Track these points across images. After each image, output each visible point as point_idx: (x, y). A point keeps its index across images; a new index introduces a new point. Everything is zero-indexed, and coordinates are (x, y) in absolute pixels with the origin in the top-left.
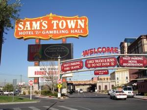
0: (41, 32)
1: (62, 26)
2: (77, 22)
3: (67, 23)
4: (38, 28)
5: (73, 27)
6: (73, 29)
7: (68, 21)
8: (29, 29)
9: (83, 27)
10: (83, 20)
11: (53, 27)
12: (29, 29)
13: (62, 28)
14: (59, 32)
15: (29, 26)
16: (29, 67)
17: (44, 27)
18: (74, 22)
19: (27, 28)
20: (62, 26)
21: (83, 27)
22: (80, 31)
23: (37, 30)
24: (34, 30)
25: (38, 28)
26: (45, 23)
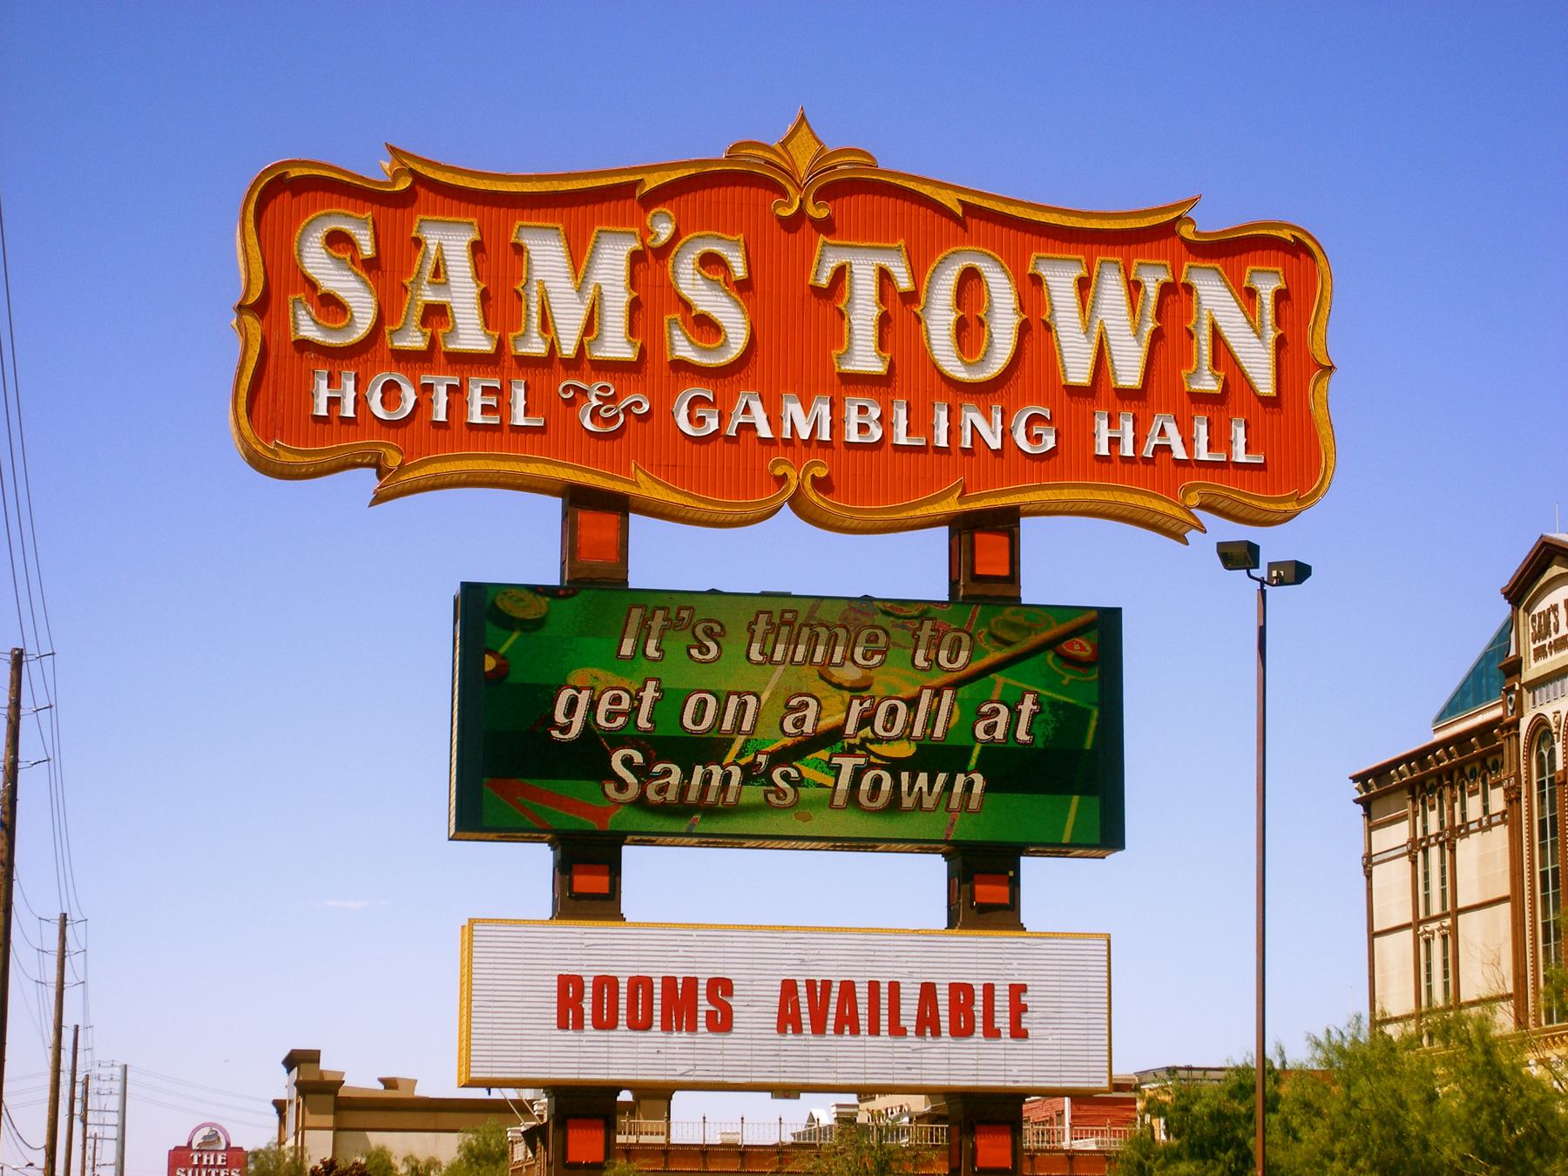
0: (661, 414)
1: (969, 332)
2: (1176, 294)
3: (1031, 290)
4: (616, 345)
5: (1129, 371)
6: (1125, 395)
7: (1061, 281)
8: (471, 336)
9: (1265, 384)
10: (1266, 288)
11: (836, 329)
12: (471, 336)
13: (955, 368)
14: (920, 422)
15: (463, 295)
16: (1022, 858)
17: (706, 327)
18: (1134, 287)
19: (436, 314)
20: (969, 332)
21: (1265, 384)
22: (1219, 440)
23: (579, 363)
24: (550, 362)
25: (616, 345)
26: (710, 262)
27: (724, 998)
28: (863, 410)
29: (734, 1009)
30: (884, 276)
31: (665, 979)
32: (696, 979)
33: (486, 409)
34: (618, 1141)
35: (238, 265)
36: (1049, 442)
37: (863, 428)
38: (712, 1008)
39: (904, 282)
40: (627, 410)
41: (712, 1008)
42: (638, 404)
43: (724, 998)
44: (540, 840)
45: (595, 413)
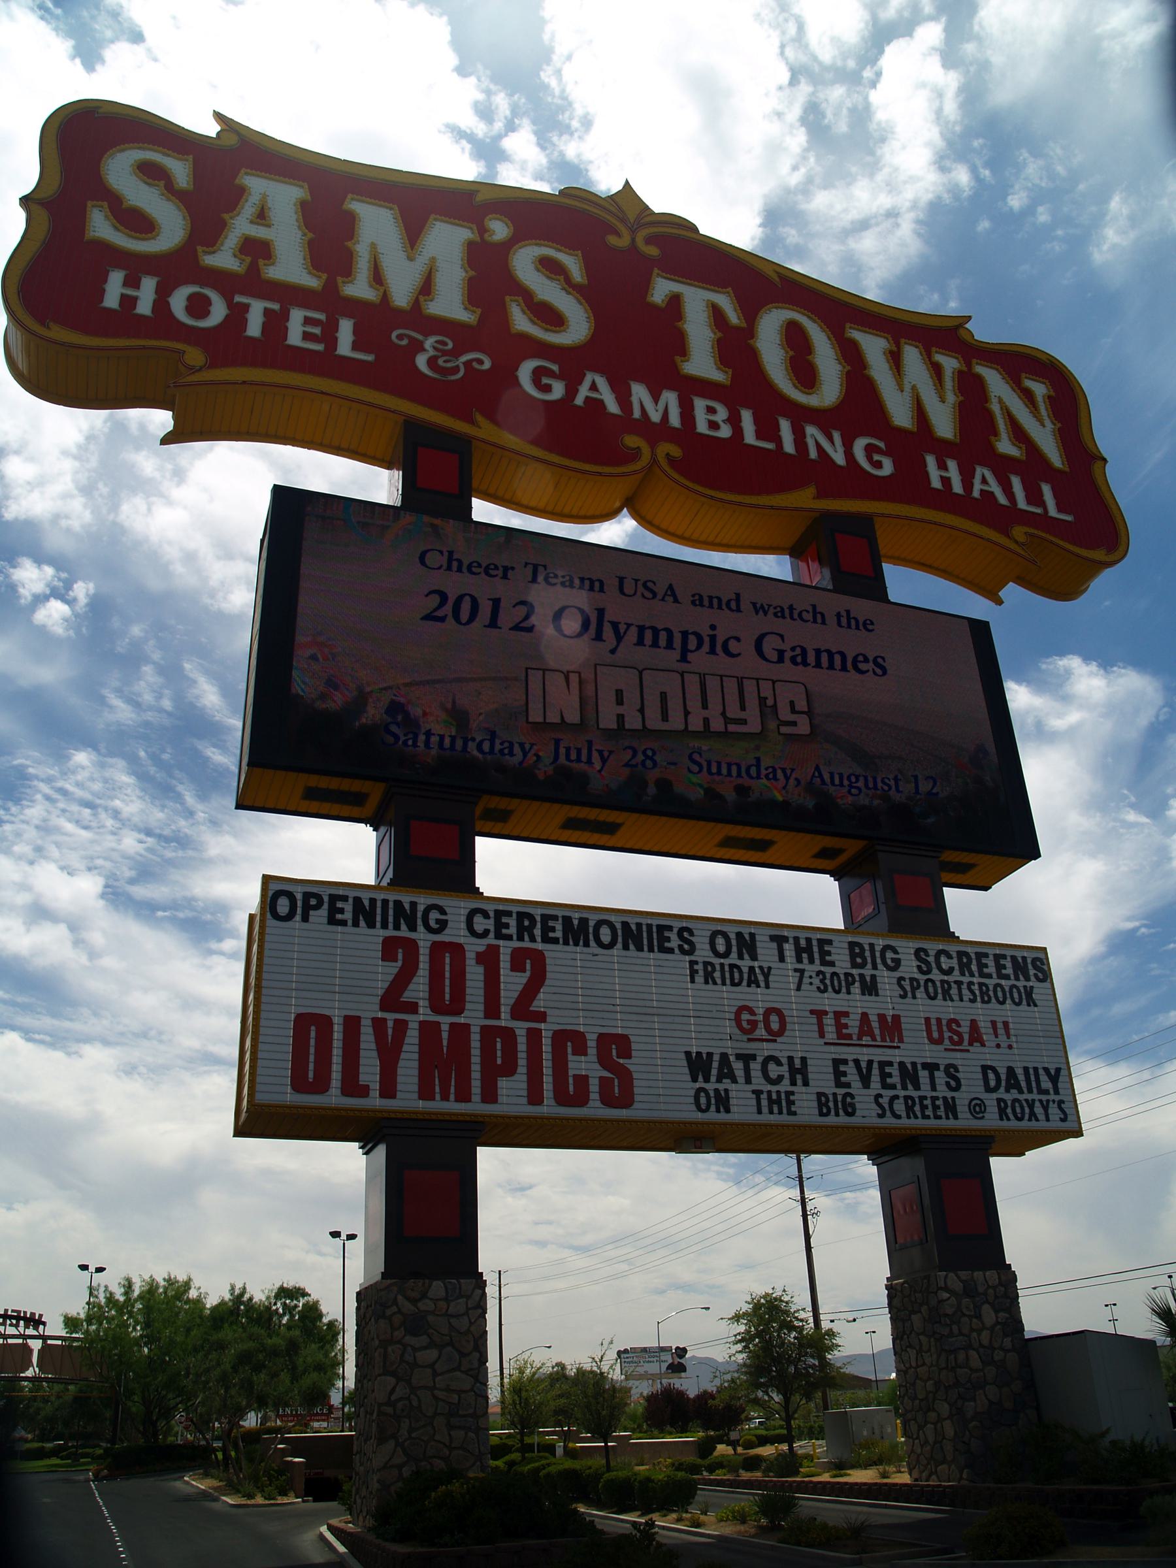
11: (680, 346)
27: (621, 1061)
28: (711, 410)
29: (635, 1075)
30: (717, 315)
31: (347, 1019)
32: (359, 1018)
33: (307, 336)
34: (323, 345)
35: (440, 1081)
36: (887, 468)
37: (714, 425)
38: (606, 1074)
39: (733, 317)
40: (467, 364)
41: (606, 1074)
42: (481, 362)
43: (621, 1061)
44: (168, 304)
45: (432, 362)
